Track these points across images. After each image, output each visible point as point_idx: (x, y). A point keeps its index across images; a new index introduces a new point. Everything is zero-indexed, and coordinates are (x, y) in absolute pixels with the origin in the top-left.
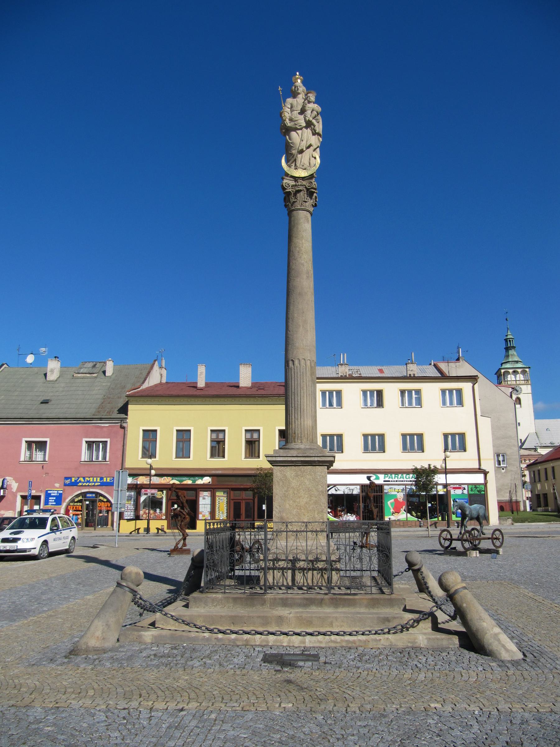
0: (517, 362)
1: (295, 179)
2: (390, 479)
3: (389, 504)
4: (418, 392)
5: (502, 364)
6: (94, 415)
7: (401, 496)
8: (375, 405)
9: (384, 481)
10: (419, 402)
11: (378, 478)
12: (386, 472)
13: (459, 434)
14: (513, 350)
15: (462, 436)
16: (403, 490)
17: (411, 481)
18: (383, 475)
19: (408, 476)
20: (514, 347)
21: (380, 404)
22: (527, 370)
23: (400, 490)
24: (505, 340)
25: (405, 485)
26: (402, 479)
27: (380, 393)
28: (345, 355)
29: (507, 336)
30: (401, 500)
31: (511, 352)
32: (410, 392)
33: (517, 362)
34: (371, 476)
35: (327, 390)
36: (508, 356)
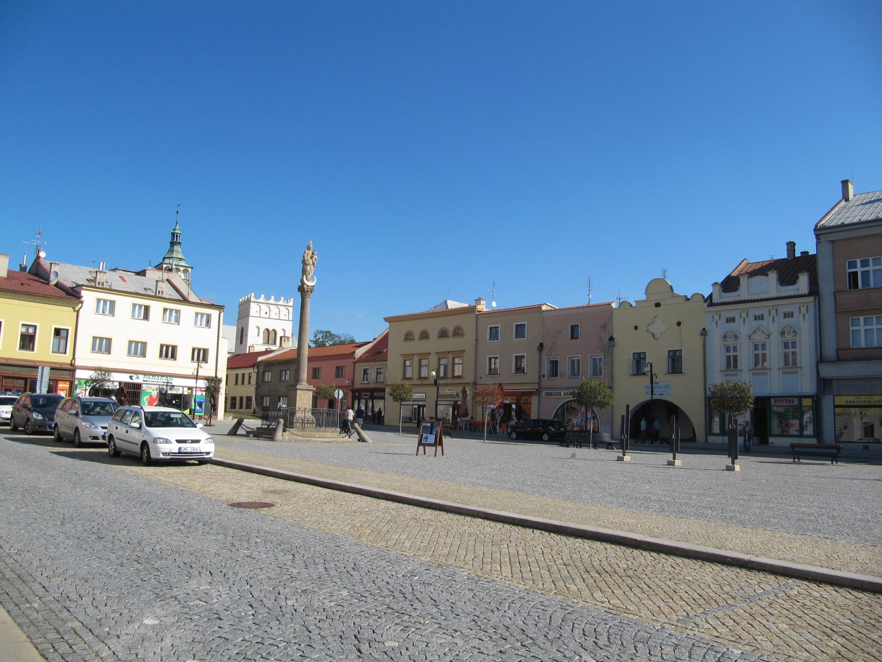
0: (181, 259)
1: (307, 286)
2: (148, 380)
3: (145, 399)
4: (178, 312)
5: (164, 258)
6: (861, 439)
7: (155, 394)
8: (142, 317)
9: (143, 381)
10: (177, 320)
11: (138, 378)
12: (145, 374)
13: (106, 339)
14: (178, 246)
15: (205, 351)
16: (157, 389)
17: (164, 382)
18: (143, 376)
19: (162, 378)
20: (180, 243)
21: (146, 317)
22: (190, 270)
23: (155, 389)
24: (172, 233)
25: (160, 385)
26: (157, 380)
27: (147, 308)
28: (105, 263)
29: (174, 230)
30: (155, 397)
31: (176, 248)
32: (171, 310)
33: (181, 259)
34: (132, 376)
35: (102, 299)
36: (172, 251)
